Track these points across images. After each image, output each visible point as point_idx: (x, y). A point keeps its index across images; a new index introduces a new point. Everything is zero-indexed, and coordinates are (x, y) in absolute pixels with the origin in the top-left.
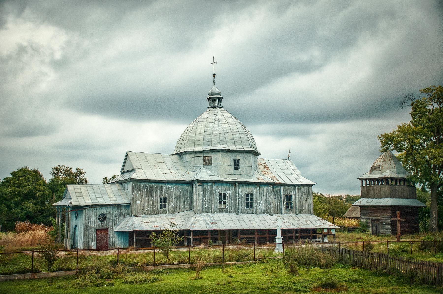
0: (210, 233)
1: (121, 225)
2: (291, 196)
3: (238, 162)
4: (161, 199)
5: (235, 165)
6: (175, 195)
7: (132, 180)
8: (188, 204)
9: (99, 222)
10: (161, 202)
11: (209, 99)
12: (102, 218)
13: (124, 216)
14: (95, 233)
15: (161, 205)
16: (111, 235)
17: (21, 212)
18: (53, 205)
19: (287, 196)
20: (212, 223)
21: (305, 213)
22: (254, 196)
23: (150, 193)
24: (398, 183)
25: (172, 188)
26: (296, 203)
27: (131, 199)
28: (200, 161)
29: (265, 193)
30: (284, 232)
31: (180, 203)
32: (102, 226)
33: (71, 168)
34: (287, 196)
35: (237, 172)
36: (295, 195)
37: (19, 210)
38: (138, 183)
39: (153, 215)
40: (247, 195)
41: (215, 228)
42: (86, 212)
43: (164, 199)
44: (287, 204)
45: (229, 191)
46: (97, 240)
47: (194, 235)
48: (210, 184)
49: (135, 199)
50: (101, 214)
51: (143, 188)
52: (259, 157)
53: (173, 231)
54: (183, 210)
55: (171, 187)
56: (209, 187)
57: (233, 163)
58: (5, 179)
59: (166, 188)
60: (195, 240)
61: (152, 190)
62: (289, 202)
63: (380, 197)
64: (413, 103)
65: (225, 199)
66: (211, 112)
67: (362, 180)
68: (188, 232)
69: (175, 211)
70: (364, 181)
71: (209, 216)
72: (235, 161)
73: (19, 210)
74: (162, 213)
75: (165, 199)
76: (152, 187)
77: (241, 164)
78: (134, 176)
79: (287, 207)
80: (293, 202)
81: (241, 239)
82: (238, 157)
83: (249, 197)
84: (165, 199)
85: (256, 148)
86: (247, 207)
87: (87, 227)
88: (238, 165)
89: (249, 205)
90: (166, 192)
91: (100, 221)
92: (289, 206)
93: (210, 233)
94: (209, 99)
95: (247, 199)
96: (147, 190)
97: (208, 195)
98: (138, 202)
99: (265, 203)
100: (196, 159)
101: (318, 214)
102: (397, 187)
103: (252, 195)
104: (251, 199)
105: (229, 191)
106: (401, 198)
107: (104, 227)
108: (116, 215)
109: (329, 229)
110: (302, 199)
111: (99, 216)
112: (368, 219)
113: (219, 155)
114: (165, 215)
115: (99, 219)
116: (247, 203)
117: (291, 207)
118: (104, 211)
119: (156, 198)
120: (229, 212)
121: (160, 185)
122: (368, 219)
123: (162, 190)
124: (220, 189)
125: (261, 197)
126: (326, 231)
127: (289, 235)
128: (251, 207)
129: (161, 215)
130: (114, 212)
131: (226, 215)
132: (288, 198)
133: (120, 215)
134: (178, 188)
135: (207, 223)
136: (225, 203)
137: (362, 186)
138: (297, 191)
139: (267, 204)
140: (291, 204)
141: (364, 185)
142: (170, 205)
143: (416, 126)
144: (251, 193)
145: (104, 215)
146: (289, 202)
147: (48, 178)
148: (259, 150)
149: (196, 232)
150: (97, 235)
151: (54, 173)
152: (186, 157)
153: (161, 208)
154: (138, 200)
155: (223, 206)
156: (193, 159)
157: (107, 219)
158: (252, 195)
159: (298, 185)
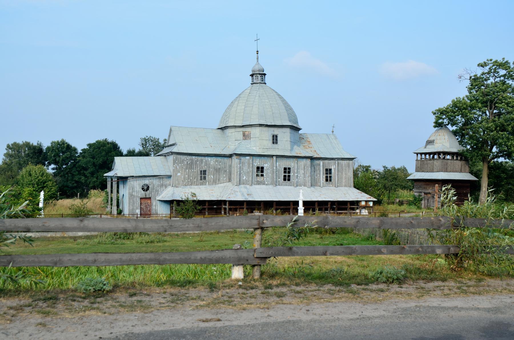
0: (291, 204)
1: (163, 195)
2: (330, 170)
3: (276, 136)
4: (201, 171)
5: (273, 139)
6: (214, 168)
7: (172, 153)
8: (228, 177)
9: (143, 192)
10: (201, 174)
11: (252, 75)
12: (145, 188)
13: (166, 187)
14: (139, 202)
15: (201, 177)
16: (154, 204)
17: (97, 181)
18: (105, 175)
19: (327, 170)
20: (248, 195)
21: (345, 186)
22: (291, 170)
23: (190, 166)
24: (455, 158)
25: (212, 161)
26: (335, 176)
27: (172, 171)
28: (240, 136)
29: (303, 167)
30: (305, 203)
31: (219, 175)
32: (146, 195)
33: (158, 139)
34: (327, 170)
35: (275, 145)
36: (335, 169)
37: (95, 179)
38: (179, 156)
39: (193, 186)
40: (285, 169)
41: (250, 199)
42: (130, 183)
43: (204, 171)
44: (327, 177)
45: (267, 165)
46: (141, 208)
47: (230, 205)
48: (248, 158)
49: (176, 171)
50: (145, 184)
51: (183, 161)
52: (300, 132)
53: (194, 201)
54: (222, 182)
55: (211, 160)
56: (247, 161)
57: (271, 138)
58: (82, 150)
59: (206, 161)
60: (230, 209)
61: (192, 163)
62: (329, 175)
63: (432, 171)
64: (471, 77)
65: (262, 172)
66: (253, 88)
67: (417, 154)
68: (225, 202)
69: (215, 182)
70: (419, 155)
71: (246, 188)
72: (273, 136)
73: (95, 179)
74: (202, 184)
75: (205, 171)
76: (192, 160)
77: (279, 139)
78: (175, 149)
79: (327, 180)
80: (333, 175)
81: (276, 210)
82: (276, 131)
83: (287, 170)
84: (205, 171)
85: (297, 122)
86: (285, 180)
87: (131, 196)
88: (276, 140)
89: (287, 178)
90: (206, 164)
91: (144, 191)
92: (328, 179)
93: (291, 204)
94: (252, 75)
95: (285, 172)
96: (187, 163)
97: (245, 168)
98: (179, 174)
99: (302, 176)
100: (236, 133)
101: (357, 186)
102: (435, 162)
103: (289, 169)
104: (289, 172)
105: (267, 165)
106: (453, 172)
107: (148, 196)
108: (158, 186)
109: (366, 202)
110: (342, 173)
111: (143, 186)
112: (421, 192)
113: (258, 129)
114: (204, 186)
115: (142, 189)
116: (285, 176)
117: (330, 180)
118: (147, 181)
119: (197, 170)
120: (267, 185)
121: (200, 158)
122: (421, 192)
123: (202, 163)
124: (258, 162)
125: (301, 170)
126: (363, 203)
127: (309, 205)
128: (289, 180)
129: (201, 186)
130: (155, 182)
131: (264, 186)
132: (328, 171)
133: (162, 185)
134: (217, 161)
135: (243, 194)
136: (262, 175)
137: (417, 160)
138: (337, 165)
139: (304, 177)
140: (330, 177)
141: (419, 158)
142: (210, 177)
143: (471, 101)
144: (289, 167)
145: (147, 185)
146: (329, 175)
147: (79, 151)
148: (300, 125)
149: (232, 203)
150: (141, 204)
151: (143, 144)
152: (228, 131)
153: (201, 179)
154: (179, 172)
155: (260, 179)
156: (233, 134)
157: (150, 189)
158: (289, 169)
159: (338, 159)
